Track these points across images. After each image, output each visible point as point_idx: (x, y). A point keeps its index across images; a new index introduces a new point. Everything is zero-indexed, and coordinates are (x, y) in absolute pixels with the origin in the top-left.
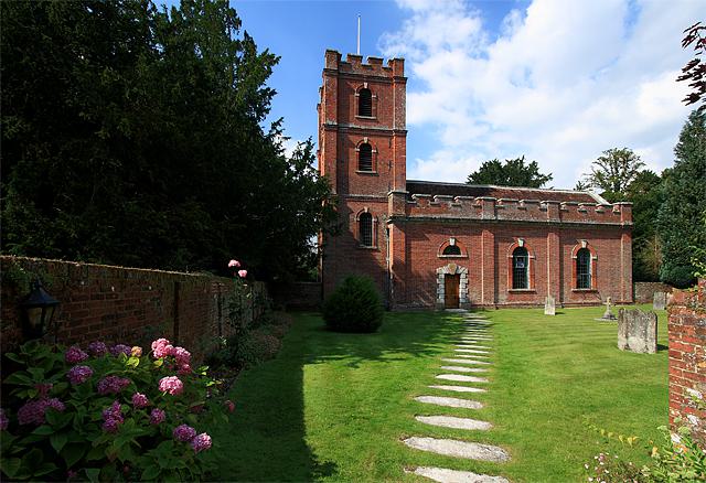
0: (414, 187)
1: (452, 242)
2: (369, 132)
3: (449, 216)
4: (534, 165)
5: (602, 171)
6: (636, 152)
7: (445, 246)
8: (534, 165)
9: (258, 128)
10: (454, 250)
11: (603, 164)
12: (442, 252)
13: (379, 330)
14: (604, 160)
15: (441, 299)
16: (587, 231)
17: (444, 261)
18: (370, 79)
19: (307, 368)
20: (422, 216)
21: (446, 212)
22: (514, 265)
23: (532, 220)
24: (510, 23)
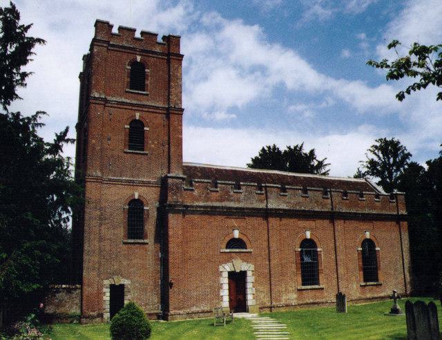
0: (194, 173)
1: (236, 234)
2: (141, 107)
3: (232, 204)
4: (312, 152)
5: (376, 159)
6: (403, 143)
7: (228, 239)
8: (312, 152)
9: (22, 128)
10: (235, 243)
11: (376, 151)
12: (224, 245)
13: (152, 333)
14: (376, 147)
15: (225, 303)
16: (385, 218)
17: (228, 258)
18: (144, 52)
19: (406, 222)
20: (201, 204)
21: (228, 200)
22: (302, 259)
23: (317, 209)
24: (266, 44)
